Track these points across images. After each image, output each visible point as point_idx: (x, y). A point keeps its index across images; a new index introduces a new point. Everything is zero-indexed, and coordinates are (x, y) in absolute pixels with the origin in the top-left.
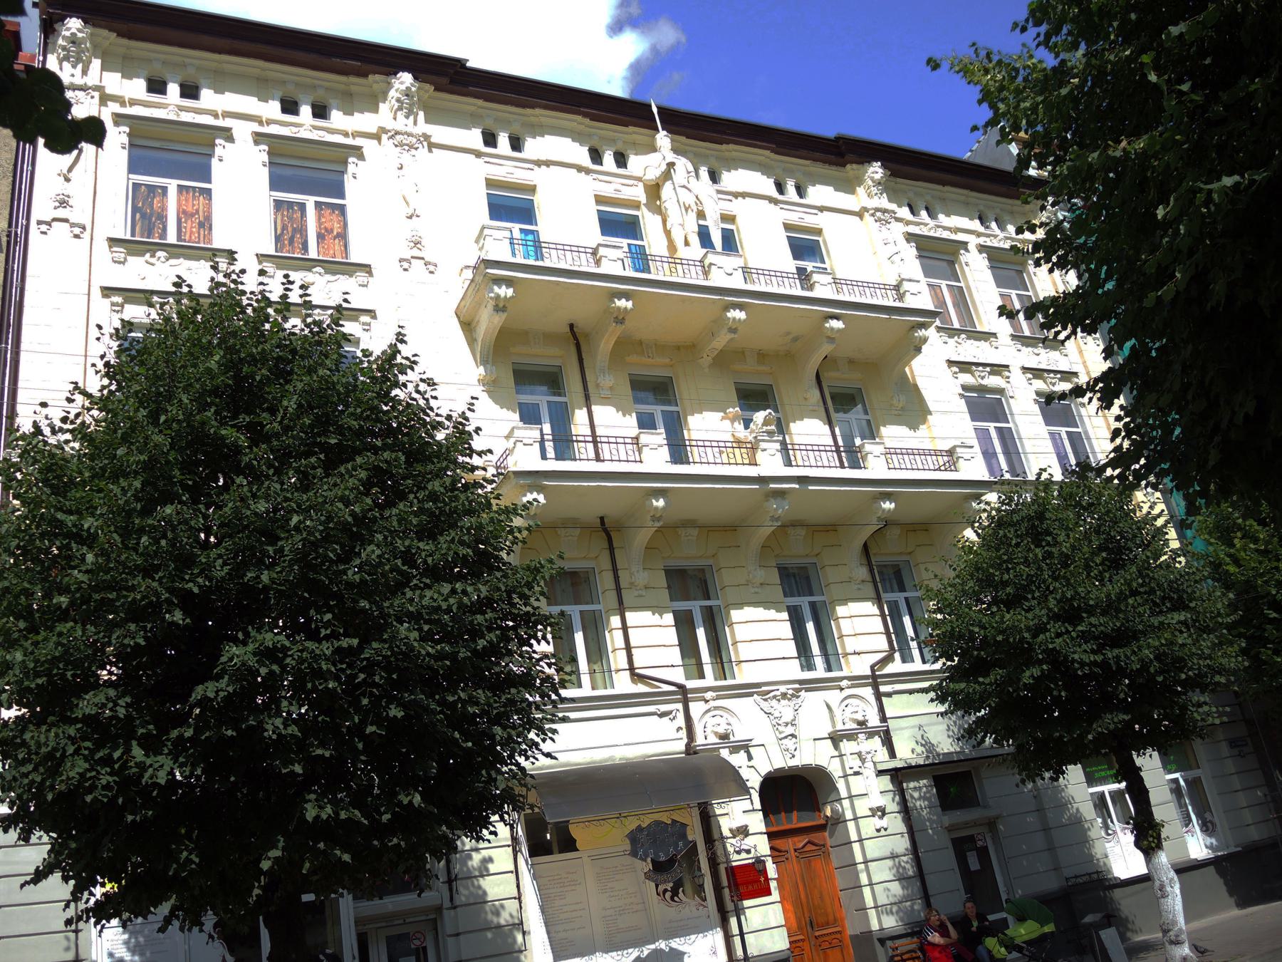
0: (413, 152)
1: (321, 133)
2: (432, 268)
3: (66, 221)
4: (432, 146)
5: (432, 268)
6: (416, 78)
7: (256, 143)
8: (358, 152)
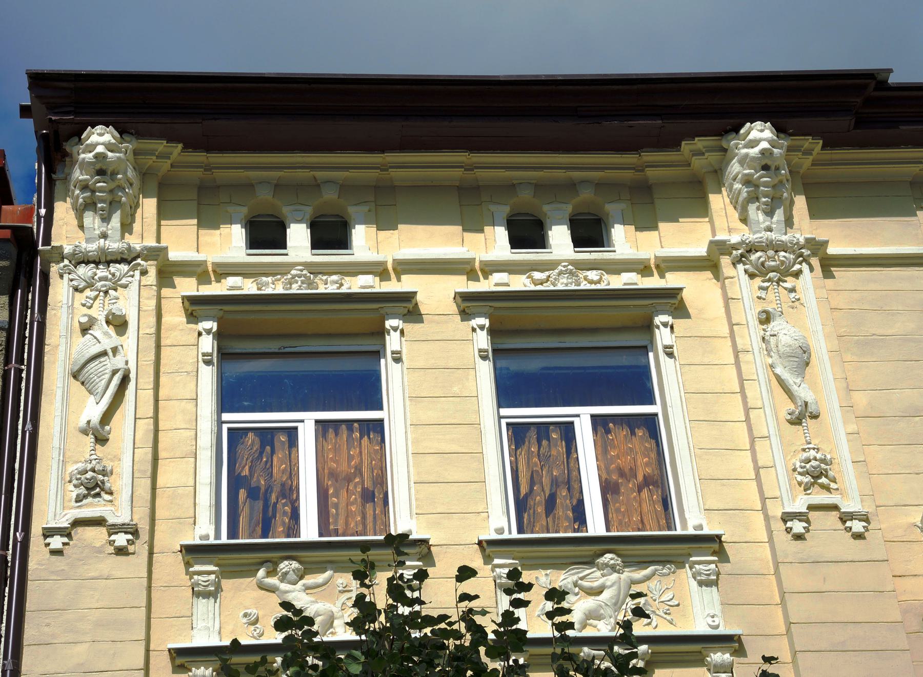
0: (790, 282)
1: (593, 275)
2: (857, 526)
3: (835, 507)
4: (829, 265)
5: (857, 526)
6: (780, 129)
7: (465, 315)
8: (672, 301)
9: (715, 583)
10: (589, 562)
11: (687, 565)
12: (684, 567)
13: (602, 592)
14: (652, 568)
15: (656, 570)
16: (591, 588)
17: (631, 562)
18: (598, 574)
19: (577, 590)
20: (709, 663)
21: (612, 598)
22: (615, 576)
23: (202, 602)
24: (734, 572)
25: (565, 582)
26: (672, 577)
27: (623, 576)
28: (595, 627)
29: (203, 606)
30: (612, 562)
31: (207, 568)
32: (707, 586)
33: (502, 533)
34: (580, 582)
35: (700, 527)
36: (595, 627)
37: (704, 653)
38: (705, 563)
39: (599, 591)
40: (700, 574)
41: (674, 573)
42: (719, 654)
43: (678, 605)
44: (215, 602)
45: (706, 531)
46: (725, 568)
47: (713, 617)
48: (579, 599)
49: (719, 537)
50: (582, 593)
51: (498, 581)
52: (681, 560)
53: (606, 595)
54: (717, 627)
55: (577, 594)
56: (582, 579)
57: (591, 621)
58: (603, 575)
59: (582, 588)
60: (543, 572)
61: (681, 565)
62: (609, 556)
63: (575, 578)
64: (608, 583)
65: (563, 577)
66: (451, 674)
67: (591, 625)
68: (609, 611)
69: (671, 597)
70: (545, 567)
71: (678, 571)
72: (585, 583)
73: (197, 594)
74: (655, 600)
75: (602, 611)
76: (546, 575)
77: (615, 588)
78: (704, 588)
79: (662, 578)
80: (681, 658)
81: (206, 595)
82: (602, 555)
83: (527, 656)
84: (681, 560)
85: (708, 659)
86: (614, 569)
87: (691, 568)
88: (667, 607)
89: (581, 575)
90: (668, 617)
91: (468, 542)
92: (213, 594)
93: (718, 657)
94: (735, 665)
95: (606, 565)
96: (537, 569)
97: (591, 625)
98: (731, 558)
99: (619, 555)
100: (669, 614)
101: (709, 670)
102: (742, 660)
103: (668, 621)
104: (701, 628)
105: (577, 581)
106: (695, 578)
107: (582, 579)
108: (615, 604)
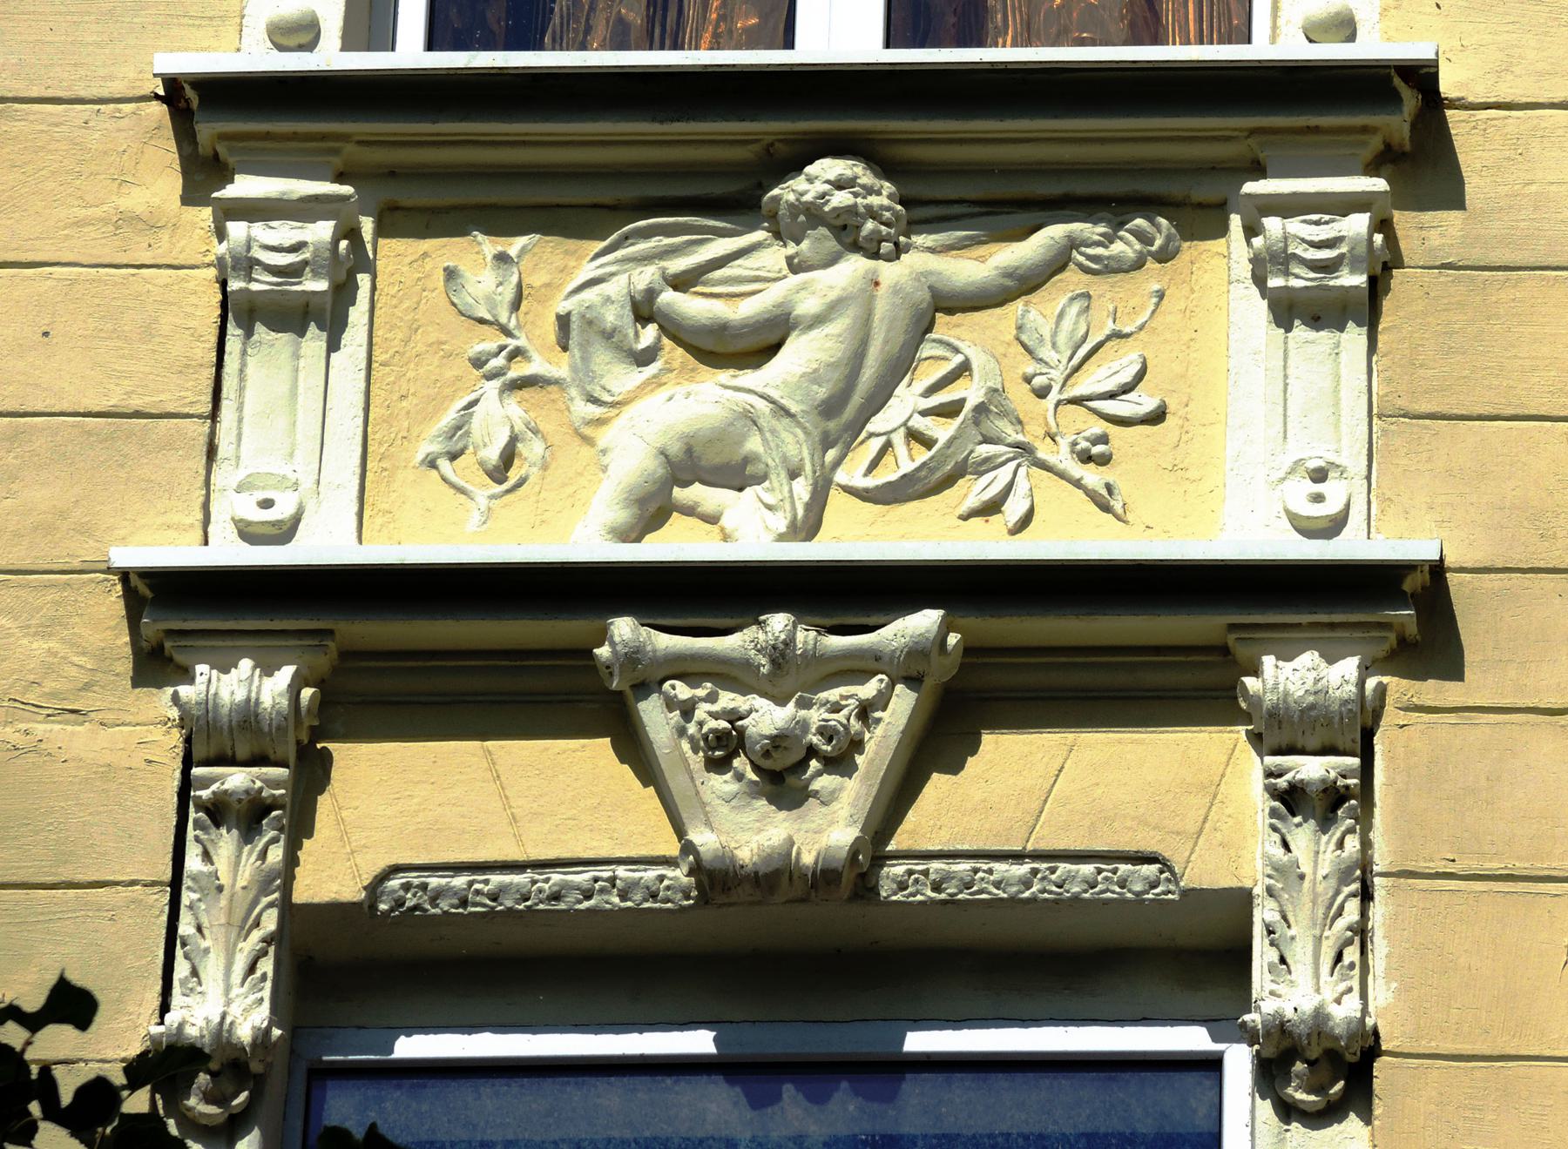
9: (1367, 308)
10: (736, 198)
11: (1235, 221)
12: (1222, 230)
13: (773, 349)
14: (1054, 233)
15: (1073, 244)
16: (721, 329)
17: (941, 199)
18: (773, 257)
19: (649, 334)
20: (1256, 701)
21: (814, 377)
22: (854, 266)
23: (271, 343)
24: (1476, 255)
25: (590, 295)
26: (1153, 277)
27: (890, 273)
28: (712, 519)
29: (270, 366)
30: (841, 199)
31: (285, 215)
32: (1316, 321)
33: (310, 46)
34: (668, 297)
35: (1345, 27)
36: (712, 519)
37: (1242, 652)
38: (1319, 209)
39: (756, 345)
40: (246, 265)
41: (1164, 256)
42: (1310, 658)
43: (1157, 417)
44: (333, 345)
45: (1371, 46)
46: (1429, 233)
47: (1319, 476)
48: (656, 382)
49: (1421, 76)
50: (673, 353)
51: (234, 285)
52: (1205, 191)
53: (801, 357)
54: (1334, 526)
55: (643, 358)
56: (682, 283)
57: (697, 493)
58: (795, 266)
59: (674, 330)
60: (489, 246)
61: (1203, 220)
62: (827, 168)
63: (645, 277)
64: (807, 306)
65: (588, 271)
66: (764, 670)
67: (689, 511)
68: (795, 444)
69: (1126, 376)
70: (501, 220)
71: (1192, 251)
72: (692, 307)
73: (240, 312)
74: (1042, 393)
75: (754, 444)
76: (502, 258)
77: (838, 325)
78: (1300, 332)
79: (1097, 286)
80: (1122, 679)
81: (291, 316)
82: (795, 165)
83: (323, 662)
84: (1205, 191)
85: (1251, 683)
86: (847, 233)
87: (1251, 231)
88: (1099, 427)
89: (678, 265)
90: (1093, 477)
91: (117, 88)
92: (310, 310)
93: (1293, 675)
94: (1391, 716)
95: (813, 215)
96: (462, 232)
97: (689, 511)
98: (1475, 185)
99: (885, 167)
100: (1104, 460)
101: (1256, 739)
102: (1431, 691)
103: (1092, 495)
104: (1248, 526)
105: (651, 293)
106: (1259, 280)
107: (682, 283)
108: (829, 408)
